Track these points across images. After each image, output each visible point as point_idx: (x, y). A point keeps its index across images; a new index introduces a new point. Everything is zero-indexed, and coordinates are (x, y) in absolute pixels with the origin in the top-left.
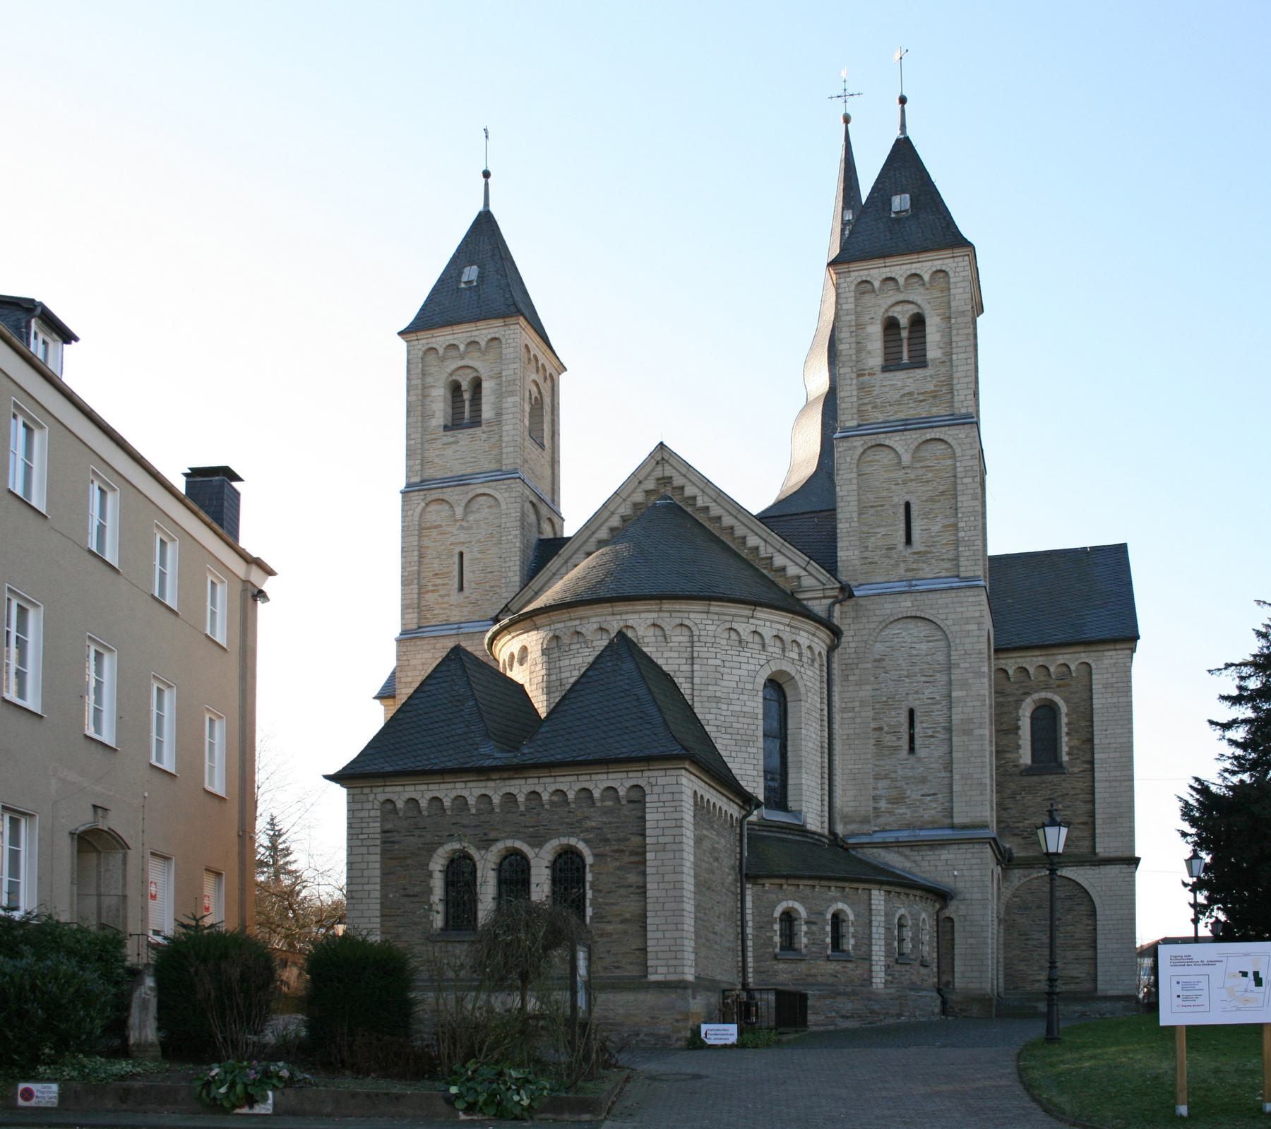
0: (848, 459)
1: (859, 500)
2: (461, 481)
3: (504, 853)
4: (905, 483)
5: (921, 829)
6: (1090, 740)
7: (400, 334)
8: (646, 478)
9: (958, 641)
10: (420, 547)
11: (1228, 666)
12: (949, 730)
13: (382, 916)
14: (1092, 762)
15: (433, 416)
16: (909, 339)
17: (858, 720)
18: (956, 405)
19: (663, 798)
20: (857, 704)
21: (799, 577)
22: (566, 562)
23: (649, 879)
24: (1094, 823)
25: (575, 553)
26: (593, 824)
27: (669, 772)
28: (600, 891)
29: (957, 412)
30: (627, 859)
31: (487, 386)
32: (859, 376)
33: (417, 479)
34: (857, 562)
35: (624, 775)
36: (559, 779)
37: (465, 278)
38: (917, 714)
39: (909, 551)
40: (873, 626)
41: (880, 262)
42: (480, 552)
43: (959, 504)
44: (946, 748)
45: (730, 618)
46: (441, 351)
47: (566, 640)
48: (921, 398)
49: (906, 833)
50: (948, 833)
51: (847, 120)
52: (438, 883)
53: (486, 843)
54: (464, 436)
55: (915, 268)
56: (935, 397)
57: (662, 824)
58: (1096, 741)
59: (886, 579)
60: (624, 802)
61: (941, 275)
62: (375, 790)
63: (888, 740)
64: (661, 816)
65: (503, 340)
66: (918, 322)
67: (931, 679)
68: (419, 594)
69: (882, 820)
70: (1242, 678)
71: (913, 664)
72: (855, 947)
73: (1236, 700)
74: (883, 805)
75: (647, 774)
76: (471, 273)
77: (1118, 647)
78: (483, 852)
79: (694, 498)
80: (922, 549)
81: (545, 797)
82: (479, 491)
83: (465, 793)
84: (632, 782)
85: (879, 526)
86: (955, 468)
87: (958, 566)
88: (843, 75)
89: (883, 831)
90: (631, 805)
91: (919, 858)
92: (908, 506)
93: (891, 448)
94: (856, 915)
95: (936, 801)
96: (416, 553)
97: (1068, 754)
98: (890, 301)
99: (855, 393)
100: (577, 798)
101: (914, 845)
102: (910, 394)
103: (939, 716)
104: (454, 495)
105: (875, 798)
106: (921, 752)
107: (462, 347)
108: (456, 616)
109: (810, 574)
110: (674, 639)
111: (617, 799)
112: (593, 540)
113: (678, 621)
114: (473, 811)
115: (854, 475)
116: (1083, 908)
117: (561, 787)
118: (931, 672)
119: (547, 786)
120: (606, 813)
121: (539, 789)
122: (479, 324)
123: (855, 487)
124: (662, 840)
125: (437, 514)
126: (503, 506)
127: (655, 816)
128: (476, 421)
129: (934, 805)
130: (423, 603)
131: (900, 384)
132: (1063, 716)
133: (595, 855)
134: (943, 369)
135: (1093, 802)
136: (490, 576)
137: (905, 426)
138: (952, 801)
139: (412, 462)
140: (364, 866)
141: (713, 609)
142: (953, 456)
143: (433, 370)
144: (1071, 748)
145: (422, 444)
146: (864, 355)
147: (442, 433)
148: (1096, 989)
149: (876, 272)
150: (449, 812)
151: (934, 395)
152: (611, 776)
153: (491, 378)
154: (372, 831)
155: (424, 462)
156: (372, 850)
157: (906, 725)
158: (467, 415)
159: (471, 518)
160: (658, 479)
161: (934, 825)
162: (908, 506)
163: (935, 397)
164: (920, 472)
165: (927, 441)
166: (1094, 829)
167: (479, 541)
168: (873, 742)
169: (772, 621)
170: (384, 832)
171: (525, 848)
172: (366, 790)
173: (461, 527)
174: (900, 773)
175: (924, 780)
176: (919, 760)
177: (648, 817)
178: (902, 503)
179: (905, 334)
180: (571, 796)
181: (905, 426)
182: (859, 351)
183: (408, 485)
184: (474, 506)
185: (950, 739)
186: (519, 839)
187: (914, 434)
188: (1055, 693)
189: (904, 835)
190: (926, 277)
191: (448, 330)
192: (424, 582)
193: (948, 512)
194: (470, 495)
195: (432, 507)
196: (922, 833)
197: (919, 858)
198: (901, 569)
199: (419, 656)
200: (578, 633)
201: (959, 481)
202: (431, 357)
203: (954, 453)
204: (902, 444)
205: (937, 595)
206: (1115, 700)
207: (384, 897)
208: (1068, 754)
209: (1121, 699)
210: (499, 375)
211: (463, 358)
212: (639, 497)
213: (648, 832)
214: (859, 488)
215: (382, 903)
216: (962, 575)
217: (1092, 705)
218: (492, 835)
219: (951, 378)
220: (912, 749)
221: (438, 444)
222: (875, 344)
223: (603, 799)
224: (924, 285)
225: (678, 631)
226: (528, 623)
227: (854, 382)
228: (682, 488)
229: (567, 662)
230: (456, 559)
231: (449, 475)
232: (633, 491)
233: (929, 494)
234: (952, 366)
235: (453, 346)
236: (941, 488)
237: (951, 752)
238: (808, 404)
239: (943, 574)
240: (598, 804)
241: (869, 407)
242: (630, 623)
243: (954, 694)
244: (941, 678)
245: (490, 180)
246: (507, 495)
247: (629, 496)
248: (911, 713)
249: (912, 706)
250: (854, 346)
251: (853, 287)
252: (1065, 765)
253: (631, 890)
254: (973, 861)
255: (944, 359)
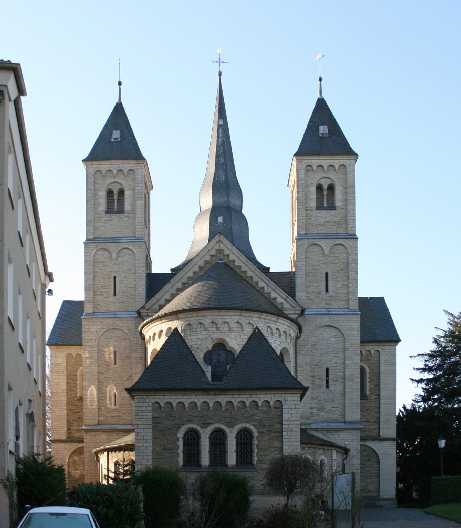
0: (301, 249)
1: (305, 269)
2: (115, 240)
3: (214, 430)
4: (326, 263)
5: (331, 423)
6: (379, 385)
7: (83, 161)
8: (211, 249)
9: (348, 338)
10: (94, 272)
11: (419, 355)
12: (344, 378)
13: (153, 459)
14: (379, 395)
15: (99, 205)
16: (327, 195)
17: (305, 372)
18: (349, 229)
19: (291, 407)
20: (304, 364)
21: (282, 303)
22: (173, 286)
23: (284, 444)
24: (379, 423)
25: (177, 282)
26: (258, 418)
27: (294, 395)
28: (261, 449)
29: (349, 232)
30: (273, 434)
31: (127, 193)
32: (306, 210)
33: (92, 237)
34: (304, 298)
35: (273, 395)
36: (241, 396)
37: (114, 136)
38: (330, 371)
39: (327, 295)
40: (312, 328)
41: (316, 157)
42: (125, 277)
43: (350, 276)
44: (342, 387)
45: (268, 321)
46: (104, 173)
47: (195, 326)
48: (333, 224)
49: (325, 424)
50: (343, 425)
51: (220, 74)
52: (181, 443)
53: (205, 425)
54: (115, 217)
55: (332, 162)
56: (339, 224)
57: (290, 419)
58: (381, 386)
59: (317, 307)
60: (272, 408)
61: (343, 167)
62: (149, 397)
63: (317, 381)
64: (290, 415)
65: (136, 171)
66: (331, 188)
67: (336, 355)
68: (94, 295)
69: (314, 418)
70: (426, 361)
71: (329, 347)
72: (327, 475)
73: (423, 370)
74: (315, 411)
75: (283, 395)
76: (116, 134)
77: (391, 344)
78: (204, 429)
79: (234, 261)
80: (333, 295)
81: (235, 404)
82: (124, 247)
83: (196, 401)
84: (276, 399)
85: (314, 282)
86: (348, 258)
87: (348, 304)
88: (219, 51)
89: (315, 423)
90: (275, 410)
91: (330, 436)
92: (327, 274)
93: (319, 245)
94: (328, 461)
95: (338, 410)
96: (92, 275)
97: (369, 391)
98: (321, 176)
99: (304, 218)
100: (250, 405)
101: (328, 430)
102: (328, 221)
103: (340, 372)
104: (112, 247)
105: (311, 408)
106: (332, 388)
107: (115, 172)
108: (112, 308)
109: (288, 302)
110: (246, 329)
111: (270, 406)
112: (186, 277)
113: (248, 321)
114: (199, 409)
115: (304, 257)
116: (374, 460)
117: (243, 400)
118: (336, 352)
119: (236, 399)
120: (264, 413)
121: (232, 400)
122: (124, 161)
123: (304, 263)
124: (290, 426)
125: (103, 256)
126: (137, 255)
127: (288, 415)
128: (121, 211)
129: (337, 412)
130: (95, 300)
131: (324, 216)
132: (367, 374)
133: (259, 432)
134: (343, 212)
135: (379, 413)
136: (129, 289)
137: (326, 236)
138: (345, 411)
139: (89, 228)
140: (144, 434)
141: (263, 317)
142: (347, 253)
143: (99, 181)
144: (370, 388)
145: (94, 219)
146: (308, 200)
147: (104, 215)
148: (379, 495)
149: (315, 161)
150: (187, 409)
151: (339, 223)
152: (266, 395)
153: (130, 189)
154: (148, 417)
155: (95, 229)
156: (148, 426)
157: (325, 375)
158: (116, 206)
159: (120, 259)
160: (217, 250)
161: (337, 421)
162: (327, 274)
163: (339, 224)
164: (333, 259)
165: (336, 245)
166: (379, 425)
167: (124, 271)
168: (311, 382)
169: (284, 324)
170: (154, 418)
171: (225, 428)
172: (145, 397)
173: (115, 264)
174: (322, 397)
175: (332, 401)
176: (331, 391)
177: (284, 415)
178: (325, 272)
179: (325, 193)
180: (248, 404)
181: (326, 236)
182: (306, 198)
183: (87, 240)
184: (122, 254)
185: (345, 383)
186: (222, 424)
187: (331, 241)
188: (364, 363)
189: (325, 425)
190: (337, 167)
191: (108, 162)
192: (96, 290)
193: (344, 278)
194: (120, 248)
195: (100, 252)
196: (332, 425)
197: (330, 436)
198: (324, 303)
199: (94, 327)
200: (200, 323)
201: (350, 265)
202: (98, 175)
203: (347, 251)
204: (326, 245)
205: (340, 317)
206: (389, 368)
207: (154, 450)
208: (369, 391)
209: (392, 368)
210: (134, 189)
211: (114, 177)
212: (208, 258)
213: (284, 422)
214: (306, 264)
215: (153, 452)
216: (350, 308)
217: (380, 370)
218: (209, 421)
219: (346, 216)
220: (327, 386)
221: (102, 220)
222: (313, 196)
223: (262, 406)
224: (335, 171)
225: (248, 325)
226: (174, 316)
227: (304, 213)
228: (228, 256)
229: (195, 337)
230: (112, 279)
231: (108, 236)
232: (206, 255)
233: (337, 269)
234: (347, 210)
235: (110, 171)
236: (342, 267)
237: (345, 389)
238: (201, 213)
239: (342, 307)
240: (260, 408)
241: (310, 226)
242: (227, 320)
243: (346, 362)
244: (341, 355)
245: (122, 87)
246: (138, 250)
247: (203, 257)
248: (327, 370)
249: (328, 367)
250: (304, 195)
251: (304, 167)
252: (368, 396)
253: (276, 449)
254: (354, 438)
255: (343, 207)
